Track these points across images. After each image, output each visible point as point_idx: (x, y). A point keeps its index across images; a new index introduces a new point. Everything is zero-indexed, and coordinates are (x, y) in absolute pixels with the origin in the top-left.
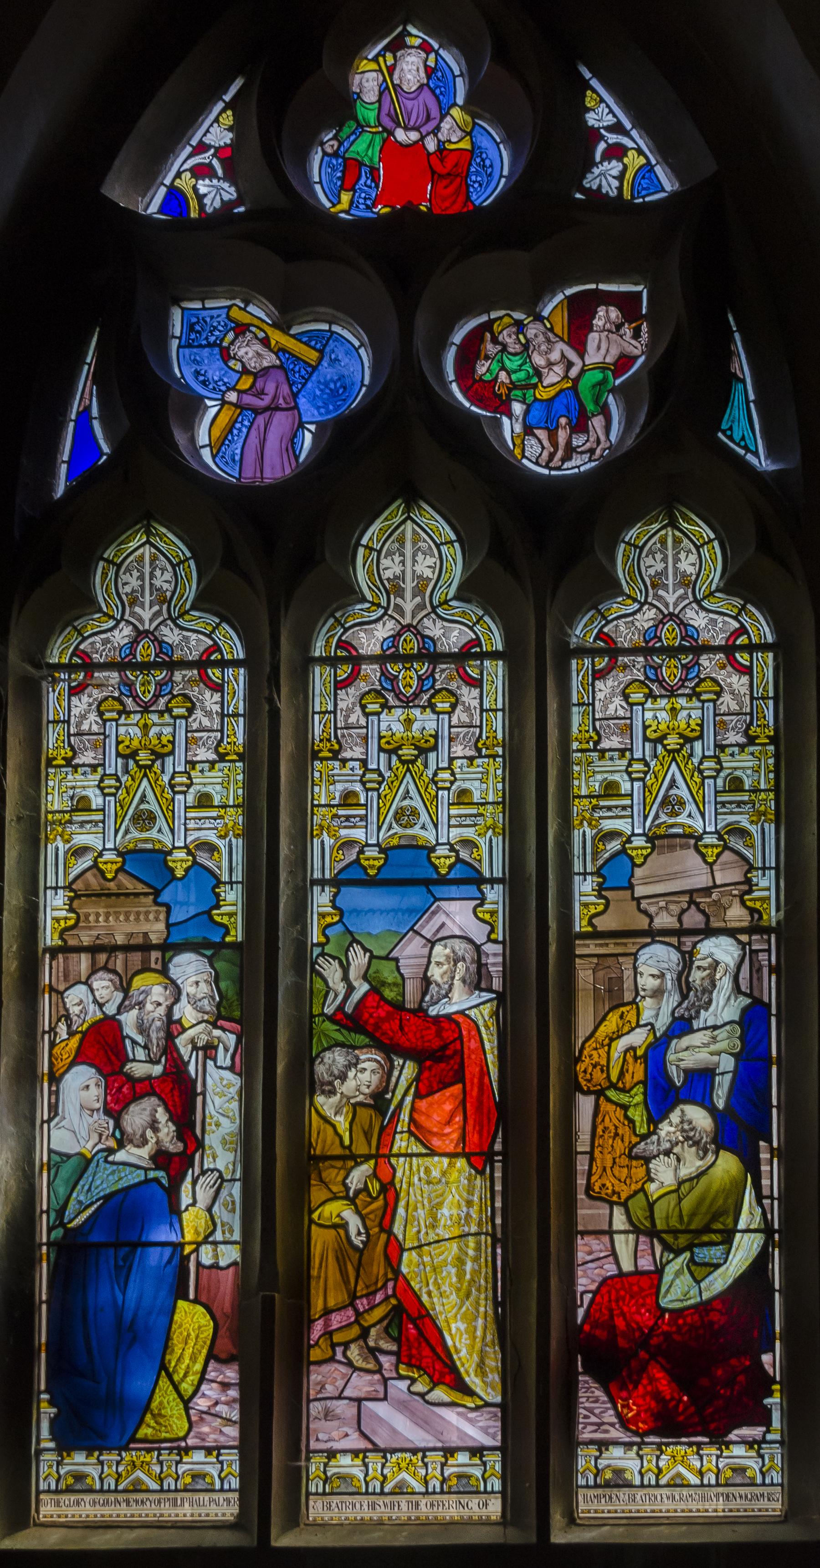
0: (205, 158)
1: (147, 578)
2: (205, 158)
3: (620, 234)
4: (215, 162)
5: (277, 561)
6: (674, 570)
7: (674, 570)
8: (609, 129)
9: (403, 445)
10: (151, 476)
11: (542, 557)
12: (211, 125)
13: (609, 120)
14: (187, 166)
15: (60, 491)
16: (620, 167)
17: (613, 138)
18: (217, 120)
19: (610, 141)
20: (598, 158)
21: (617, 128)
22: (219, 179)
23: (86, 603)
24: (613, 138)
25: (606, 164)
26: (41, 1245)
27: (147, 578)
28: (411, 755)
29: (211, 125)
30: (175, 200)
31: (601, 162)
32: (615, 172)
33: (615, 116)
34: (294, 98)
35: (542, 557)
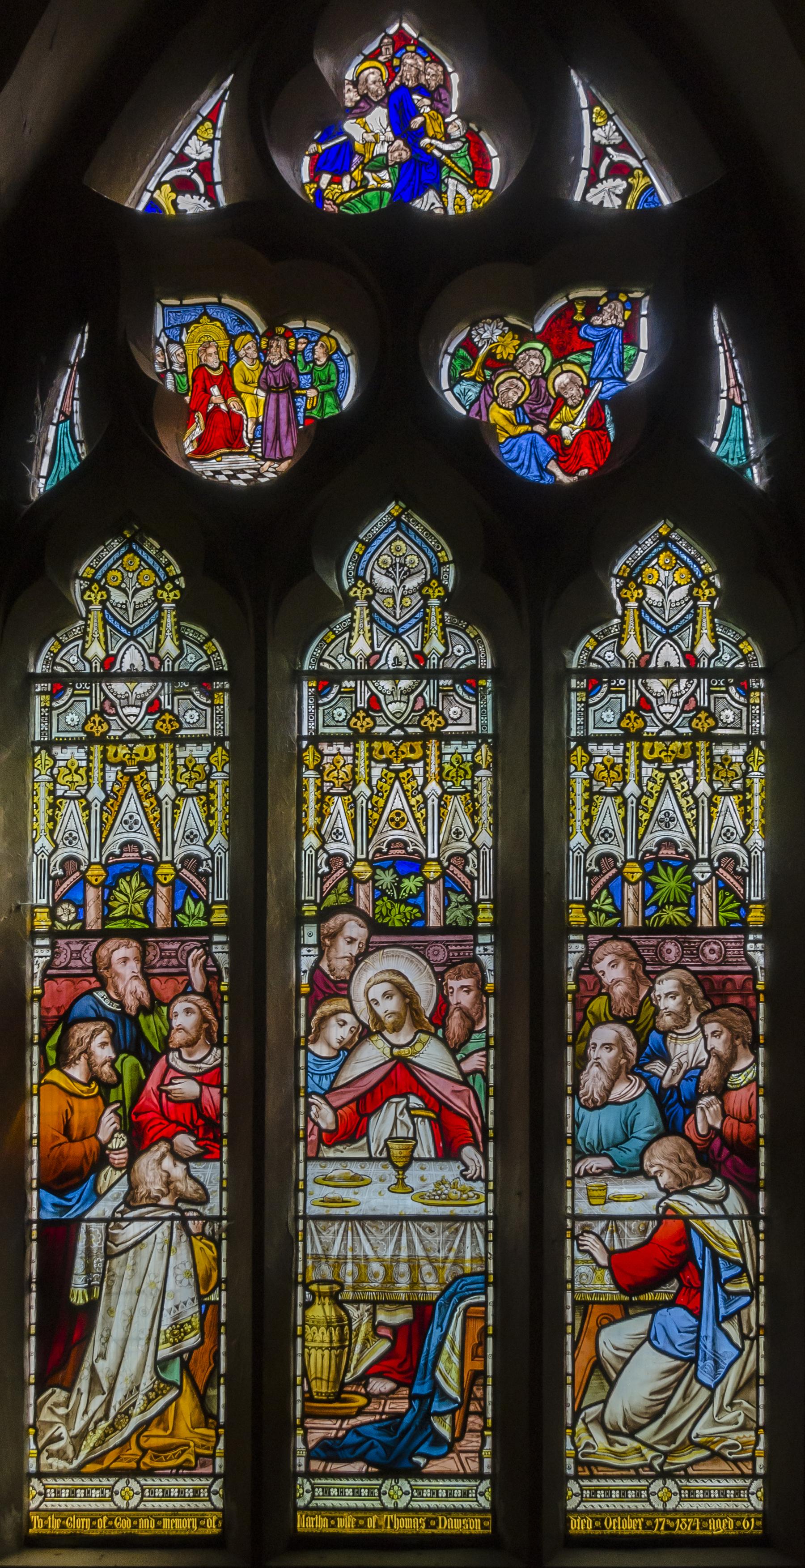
0: (183, 171)
1: (125, 608)
2: (183, 171)
3: (620, 250)
4: (196, 177)
5: (257, 577)
6: (666, 591)
7: (666, 591)
8: (615, 147)
9: (390, 448)
10: (132, 481)
11: (531, 567)
12: (190, 138)
13: (617, 139)
14: (167, 177)
15: (42, 480)
16: (624, 185)
17: (618, 157)
18: (194, 133)
19: (616, 159)
20: (602, 174)
21: (624, 147)
22: (201, 195)
23: (67, 613)
24: (618, 157)
25: (610, 180)
26: (31, 1222)
27: (125, 608)
28: (395, 787)
29: (190, 138)
30: (153, 205)
31: (606, 178)
32: (619, 191)
33: (621, 134)
34: (281, 101)
35: (531, 567)
